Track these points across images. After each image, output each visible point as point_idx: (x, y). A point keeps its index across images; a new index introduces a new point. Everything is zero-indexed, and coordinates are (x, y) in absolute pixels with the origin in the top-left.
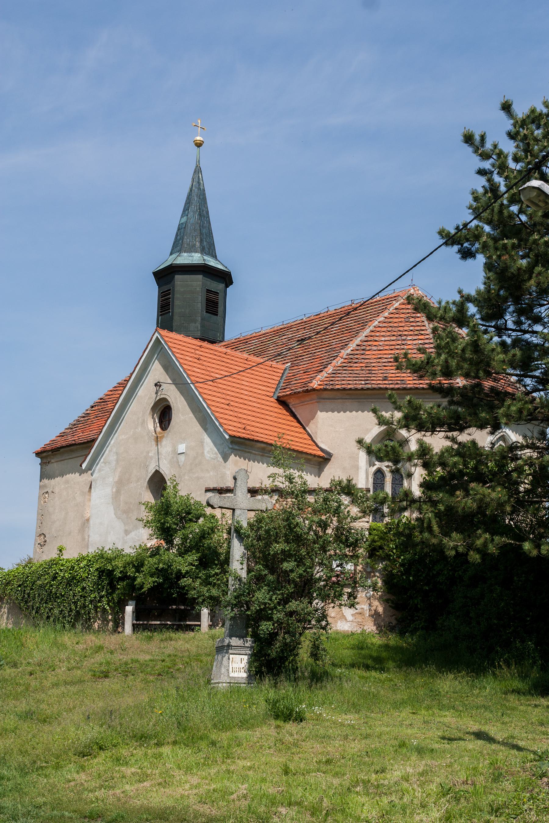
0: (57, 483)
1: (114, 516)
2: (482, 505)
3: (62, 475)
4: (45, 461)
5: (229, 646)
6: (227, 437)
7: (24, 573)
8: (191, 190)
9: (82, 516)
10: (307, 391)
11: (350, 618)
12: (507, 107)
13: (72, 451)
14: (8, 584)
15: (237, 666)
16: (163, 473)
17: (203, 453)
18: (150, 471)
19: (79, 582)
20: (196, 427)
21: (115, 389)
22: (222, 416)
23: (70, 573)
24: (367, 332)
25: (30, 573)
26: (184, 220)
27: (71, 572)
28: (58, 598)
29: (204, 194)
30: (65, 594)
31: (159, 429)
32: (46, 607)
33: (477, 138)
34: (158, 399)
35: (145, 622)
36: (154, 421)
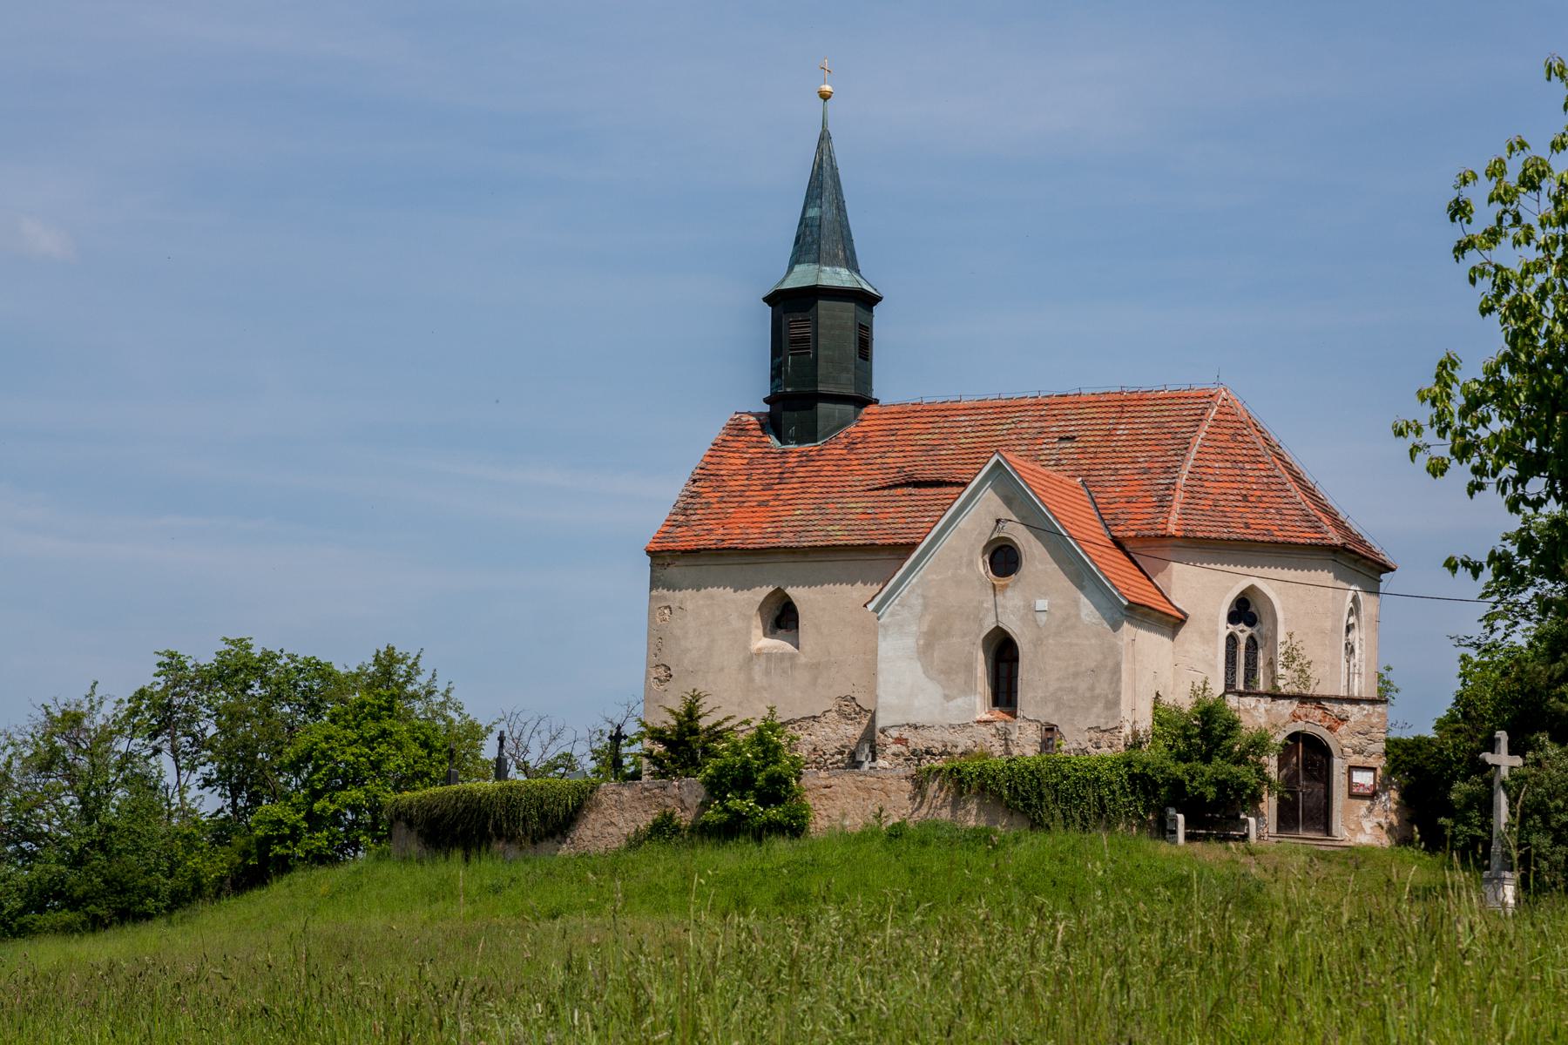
0: (692, 601)
9: (746, 648)
11: (1369, 831)
17: (1078, 616)
24: (1193, 454)
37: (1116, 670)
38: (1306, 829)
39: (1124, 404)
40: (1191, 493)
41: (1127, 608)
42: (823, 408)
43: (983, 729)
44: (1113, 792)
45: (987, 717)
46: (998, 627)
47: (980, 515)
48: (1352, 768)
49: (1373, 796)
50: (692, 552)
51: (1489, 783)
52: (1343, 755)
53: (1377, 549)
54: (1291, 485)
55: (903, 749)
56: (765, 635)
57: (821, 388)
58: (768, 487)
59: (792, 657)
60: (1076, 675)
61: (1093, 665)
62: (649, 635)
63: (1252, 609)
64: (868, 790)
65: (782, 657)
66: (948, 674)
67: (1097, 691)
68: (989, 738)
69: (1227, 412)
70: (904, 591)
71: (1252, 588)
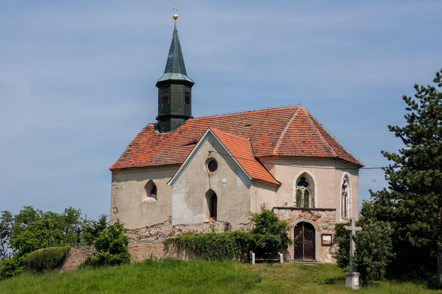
0: (123, 185)
2: (421, 229)
5: (354, 275)
6: (251, 179)
9: (141, 201)
11: (330, 258)
12: (416, 87)
13: (133, 170)
15: (356, 281)
17: (236, 184)
22: (245, 166)
24: (287, 128)
33: (408, 98)
36: (206, 166)
37: (249, 202)
38: (306, 257)
39: (267, 113)
40: (284, 141)
41: (252, 180)
42: (172, 120)
43: (206, 225)
44: (230, 246)
45: (207, 221)
46: (210, 189)
47: (205, 150)
48: (323, 235)
49: (331, 245)
50: (125, 168)
51: (348, 237)
52: (319, 230)
53: (357, 159)
54: (322, 138)
55: (181, 233)
56: (148, 196)
57: (172, 113)
58: (152, 147)
59: (155, 203)
60: (236, 205)
61: (241, 201)
62: (112, 198)
63: (306, 181)
64: (150, 247)
65: (152, 203)
66: (194, 206)
67: (243, 211)
68: (208, 228)
69: (301, 114)
70: (180, 178)
71: (305, 173)
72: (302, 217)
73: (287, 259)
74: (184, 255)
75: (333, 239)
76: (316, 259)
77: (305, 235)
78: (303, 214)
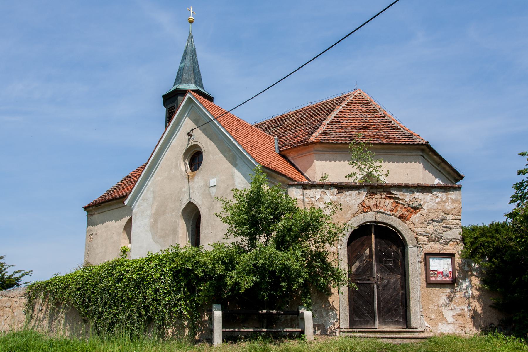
0: (99, 228)
1: (151, 240)
3: (102, 222)
4: (90, 213)
7: (83, 276)
8: (187, 48)
10: (308, 144)
11: (451, 320)
13: (110, 205)
14: (65, 288)
16: (195, 203)
18: (183, 202)
19: (149, 283)
20: (226, 164)
21: (137, 170)
23: (138, 274)
25: (90, 276)
26: (183, 65)
27: (140, 272)
28: (124, 301)
29: (195, 51)
30: (132, 298)
31: (189, 170)
32: (110, 312)
34: (189, 146)
35: (236, 330)
36: (185, 164)
38: (383, 322)
46: (190, 203)
49: (453, 283)
52: (418, 245)
72: (369, 208)
73: (330, 328)
74: (62, 322)
75: (457, 266)
76: (413, 324)
77: (379, 260)
78: (370, 202)
